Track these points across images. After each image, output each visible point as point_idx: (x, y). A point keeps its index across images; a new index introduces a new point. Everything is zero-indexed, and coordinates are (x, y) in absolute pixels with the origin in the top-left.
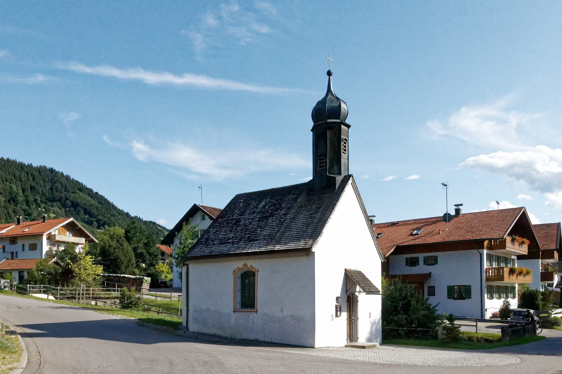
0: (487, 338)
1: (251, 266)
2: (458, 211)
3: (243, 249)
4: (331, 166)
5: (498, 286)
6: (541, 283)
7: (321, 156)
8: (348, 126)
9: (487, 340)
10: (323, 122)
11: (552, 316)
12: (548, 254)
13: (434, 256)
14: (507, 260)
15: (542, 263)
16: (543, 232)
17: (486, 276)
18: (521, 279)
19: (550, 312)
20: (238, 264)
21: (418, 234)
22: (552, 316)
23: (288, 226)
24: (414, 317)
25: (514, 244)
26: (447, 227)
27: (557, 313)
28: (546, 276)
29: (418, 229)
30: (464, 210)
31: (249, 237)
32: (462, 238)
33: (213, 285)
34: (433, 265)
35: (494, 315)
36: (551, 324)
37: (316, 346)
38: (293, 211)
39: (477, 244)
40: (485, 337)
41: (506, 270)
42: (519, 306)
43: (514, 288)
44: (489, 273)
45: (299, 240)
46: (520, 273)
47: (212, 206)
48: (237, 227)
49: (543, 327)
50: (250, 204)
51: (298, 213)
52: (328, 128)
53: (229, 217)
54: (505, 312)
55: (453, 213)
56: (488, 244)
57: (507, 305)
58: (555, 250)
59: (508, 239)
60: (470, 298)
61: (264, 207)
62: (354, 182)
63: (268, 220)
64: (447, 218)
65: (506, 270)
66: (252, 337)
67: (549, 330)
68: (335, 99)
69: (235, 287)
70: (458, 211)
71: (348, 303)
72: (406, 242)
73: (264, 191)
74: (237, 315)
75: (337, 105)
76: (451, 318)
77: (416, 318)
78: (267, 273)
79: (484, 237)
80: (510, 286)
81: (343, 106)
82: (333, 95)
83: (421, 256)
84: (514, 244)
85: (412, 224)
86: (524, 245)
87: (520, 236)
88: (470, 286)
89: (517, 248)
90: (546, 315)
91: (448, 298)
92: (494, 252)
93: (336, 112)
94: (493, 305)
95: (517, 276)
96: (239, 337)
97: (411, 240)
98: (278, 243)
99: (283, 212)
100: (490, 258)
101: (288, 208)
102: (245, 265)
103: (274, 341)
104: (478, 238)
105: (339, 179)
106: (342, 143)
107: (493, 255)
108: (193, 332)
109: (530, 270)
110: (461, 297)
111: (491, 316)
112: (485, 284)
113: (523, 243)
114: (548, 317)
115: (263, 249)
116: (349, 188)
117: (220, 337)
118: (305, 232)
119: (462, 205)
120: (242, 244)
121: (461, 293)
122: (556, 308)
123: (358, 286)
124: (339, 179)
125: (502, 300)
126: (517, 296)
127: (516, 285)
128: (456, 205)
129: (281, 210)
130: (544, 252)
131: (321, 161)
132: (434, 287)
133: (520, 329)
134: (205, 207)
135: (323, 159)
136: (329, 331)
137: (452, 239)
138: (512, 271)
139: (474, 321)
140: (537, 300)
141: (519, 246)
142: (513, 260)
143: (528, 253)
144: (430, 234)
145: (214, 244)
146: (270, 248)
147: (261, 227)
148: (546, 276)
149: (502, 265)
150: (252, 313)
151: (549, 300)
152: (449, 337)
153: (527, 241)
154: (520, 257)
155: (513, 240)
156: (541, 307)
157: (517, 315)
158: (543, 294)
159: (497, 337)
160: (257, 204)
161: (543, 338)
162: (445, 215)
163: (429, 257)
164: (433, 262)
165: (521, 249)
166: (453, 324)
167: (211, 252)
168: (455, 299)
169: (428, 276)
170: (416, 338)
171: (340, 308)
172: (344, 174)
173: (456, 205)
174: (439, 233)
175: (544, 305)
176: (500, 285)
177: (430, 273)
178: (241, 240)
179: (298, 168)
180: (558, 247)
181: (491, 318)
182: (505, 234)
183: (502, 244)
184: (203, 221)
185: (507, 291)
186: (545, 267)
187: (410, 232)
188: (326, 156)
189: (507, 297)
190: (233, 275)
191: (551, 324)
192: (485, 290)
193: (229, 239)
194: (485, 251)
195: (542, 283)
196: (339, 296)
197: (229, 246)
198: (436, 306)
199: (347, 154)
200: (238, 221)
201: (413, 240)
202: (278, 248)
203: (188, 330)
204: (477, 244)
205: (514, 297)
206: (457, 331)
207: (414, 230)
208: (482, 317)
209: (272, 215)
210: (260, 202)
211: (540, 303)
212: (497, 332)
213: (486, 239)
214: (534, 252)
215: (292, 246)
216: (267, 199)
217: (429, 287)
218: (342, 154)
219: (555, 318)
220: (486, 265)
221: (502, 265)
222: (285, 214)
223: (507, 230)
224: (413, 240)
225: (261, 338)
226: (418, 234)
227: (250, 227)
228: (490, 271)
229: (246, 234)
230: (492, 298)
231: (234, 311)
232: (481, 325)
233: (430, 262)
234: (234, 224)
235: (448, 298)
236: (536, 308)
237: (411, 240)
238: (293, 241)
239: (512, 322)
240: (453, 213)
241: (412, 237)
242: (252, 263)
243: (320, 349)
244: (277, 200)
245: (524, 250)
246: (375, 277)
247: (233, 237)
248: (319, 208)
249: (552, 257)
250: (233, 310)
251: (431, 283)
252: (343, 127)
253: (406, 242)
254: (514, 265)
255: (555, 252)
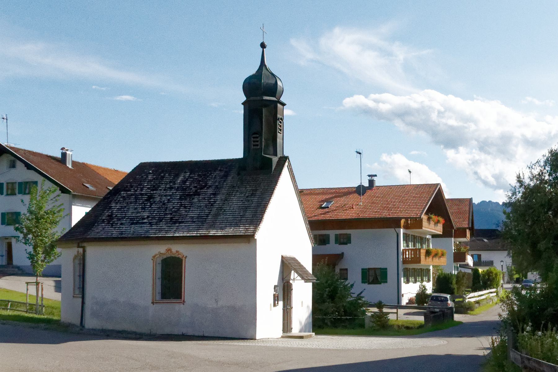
0: (408, 325)
1: (177, 252)
2: (371, 182)
3: (167, 232)
4: (267, 146)
5: (414, 269)
6: (454, 264)
7: (255, 133)
8: (283, 105)
9: (408, 328)
10: (258, 98)
11: (467, 301)
12: (461, 233)
13: (346, 234)
14: (422, 240)
15: (454, 242)
16: (456, 207)
17: (403, 258)
18: (437, 261)
19: (465, 296)
20: (161, 249)
21: (328, 207)
22: (467, 301)
23: (220, 209)
24: (341, 304)
25: (429, 223)
26: (362, 201)
27: (470, 298)
28: (459, 257)
29: (328, 201)
30: (378, 182)
31: (171, 219)
32: (377, 216)
33: (125, 271)
34: (346, 244)
35: (411, 301)
36: (464, 309)
37: (257, 338)
38: (224, 191)
39: (394, 223)
40: (406, 325)
41: (423, 252)
42: (435, 291)
43: (428, 270)
44: (406, 255)
45: (237, 225)
46: (436, 255)
47: (27, 149)
48: (151, 204)
49: (458, 312)
50: (163, 177)
51: (229, 194)
52: (262, 102)
53: (136, 191)
54: (421, 297)
55: (366, 184)
56: (405, 222)
57: (424, 289)
58: (467, 228)
59: (424, 217)
60: (386, 282)
61: (184, 182)
62: (290, 165)
63: (193, 199)
64: (360, 190)
65: (423, 252)
66: (176, 331)
67: (464, 315)
68: (270, 75)
69: (154, 274)
70: (371, 182)
71: (284, 292)
72: (315, 216)
73: (179, 162)
74: (157, 307)
75: (274, 82)
76: (380, 305)
77: (343, 306)
78: (197, 261)
79: (401, 215)
80: (425, 268)
81: (279, 83)
82: (267, 69)
83: (332, 233)
84: (429, 223)
85: (318, 194)
86: (439, 225)
87: (435, 215)
88: (386, 269)
89: (432, 227)
90: (461, 300)
91: (362, 282)
92: (411, 232)
93: (273, 89)
94: (409, 290)
95: (433, 257)
96: (160, 332)
97: (321, 214)
98: (212, 226)
99: (210, 191)
100: (406, 237)
101: (217, 187)
102: (169, 250)
103: (206, 335)
104: (395, 216)
105: (275, 160)
106: (278, 122)
107: (409, 235)
108: (89, 329)
109: (445, 251)
110: (376, 281)
111: (407, 301)
112: (401, 267)
113: (438, 222)
114: (463, 301)
115: (194, 234)
116: (285, 172)
117: (135, 333)
118: (242, 216)
119: (376, 176)
120: (163, 225)
121: (376, 276)
122: (470, 292)
123: (293, 272)
124: (275, 160)
125: (418, 284)
126: (431, 279)
127: (431, 268)
128: (369, 176)
129: (208, 188)
130: (458, 229)
131: (255, 139)
132: (347, 269)
133: (440, 315)
134: (17, 150)
135: (257, 137)
136: (268, 322)
137: (366, 215)
138: (428, 253)
139: (395, 308)
140: (451, 283)
141: (435, 225)
142: (428, 240)
143: (443, 233)
144: (342, 207)
145: (122, 224)
146: (203, 232)
147: (185, 207)
148: (459, 257)
149: (418, 246)
150: (177, 305)
151: (463, 283)
152: (378, 325)
153: (441, 219)
154: (434, 236)
155: (429, 219)
156: (456, 291)
157: (434, 300)
158: (457, 276)
159: (417, 323)
160: (174, 178)
161: (460, 323)
162: (359, 186)
163: (340, 234)
164: (345, 241)
165: (436, 228)
166: (381, 311)
167: (122, 234)
168: (369, 283)
169: (340, 257)
170: (345, 327)
171: (278, 297)
172: (279, 155)
173: (369, 176)
174: (353, 208)
175: (458, 289)
176: (416, 267)
177: (343, 253)
178: (161, 221)
179: (228, 144)
180: (470, 226)
181: (407, 304)
182: (422, 212)
183: (418, 223)
184: (13, 170)
185: (422, 274)
186: (458, 246)
187: (318, 205)
188: (261, 135)
189: (422, 281)
190: (152, 261)
191: (464, 309)
192: (401, 273)
193: (144, 219)
194: (402, 231)
195: (455, 264)
196: (276, 284)
197: (146, 227)
198: (362, 292)
199: (282, 134)
200: (150, 197)
201: (324, 214)
202: (212, 233)
203: (83, 327)
204: (394, 223)
205: (429, 281)
206: (385, 318)
207: (323, 201)
208: (398, 303)
209: (197, 194)
210: (177, 176)
211: (455, 286)
212: (421, 319)
213: (403, 218)
214: (449, 231)
215: (229, 231)
216: (186, 172)
217: (341, 270)
218: (278, 134)
219: (469, 302)
220: (402, 246)
221: (418, 246)
222: (215, 194)
223: (424, 209)
224: (324, 214)
225: (190, 332)
226: (328, 207)
227: (170, 205)
228: (407, 253)
229: (166, 214)
230: (408, 282)
231: (153, 303)
232: (401, 312)
233: (342, 240)
234: (146, 200)
235: (362, 282)
236: (451, 292)
237: (321, 214)
238: (231, 226)
239: (429, 308)
240: (366, 184)
241: (321, 211)
242: (178, 249)
243: (262, 340)
244: (199, 175)
245: (439, 230)
246: (308, 264)
247: (148, 217)
248: (256, 190)
249: (465, 236)
250: (151, 301)
251: (343, 265)
252: (279, 105)
253: (315, 216)
254: (428, 246)
255: (467, 230)
